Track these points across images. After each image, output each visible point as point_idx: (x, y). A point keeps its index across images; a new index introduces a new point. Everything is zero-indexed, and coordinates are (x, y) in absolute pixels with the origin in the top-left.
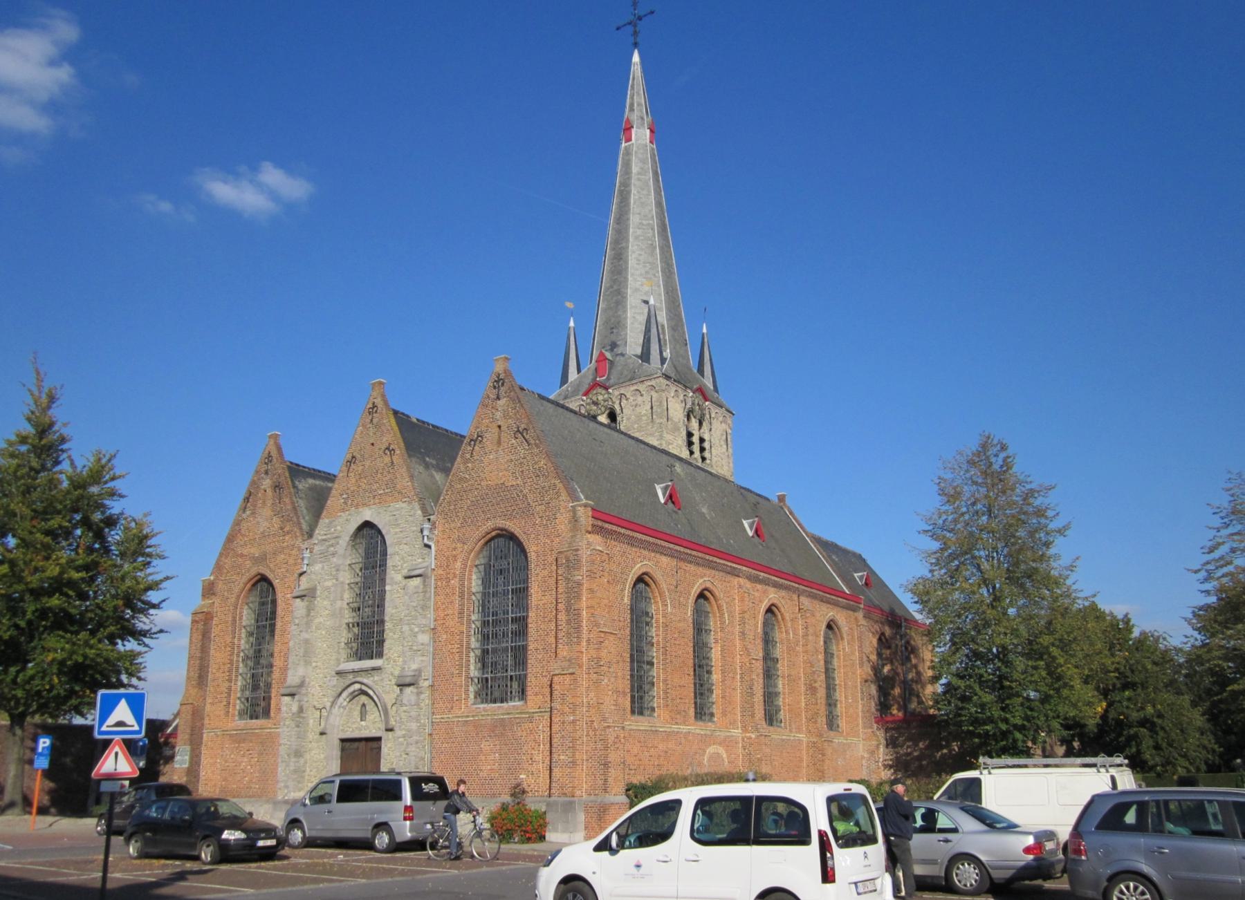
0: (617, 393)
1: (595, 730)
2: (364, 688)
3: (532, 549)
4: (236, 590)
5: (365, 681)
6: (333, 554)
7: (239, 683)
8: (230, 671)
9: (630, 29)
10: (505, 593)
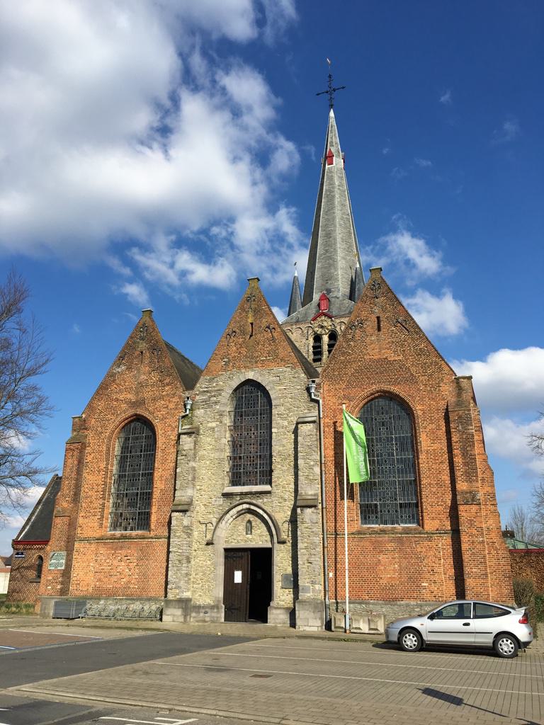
0: (338, 321)
1: (496, 549)
2: (252, 507)
3: (418, 409)
4: (111, 427)
5: (254, 502)
6: (216, 403)
7: (111, 501)
8: (104, 491)
9: (327, 96)
10: (389, 440)
